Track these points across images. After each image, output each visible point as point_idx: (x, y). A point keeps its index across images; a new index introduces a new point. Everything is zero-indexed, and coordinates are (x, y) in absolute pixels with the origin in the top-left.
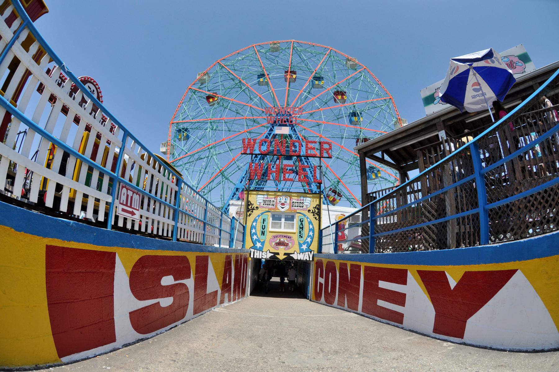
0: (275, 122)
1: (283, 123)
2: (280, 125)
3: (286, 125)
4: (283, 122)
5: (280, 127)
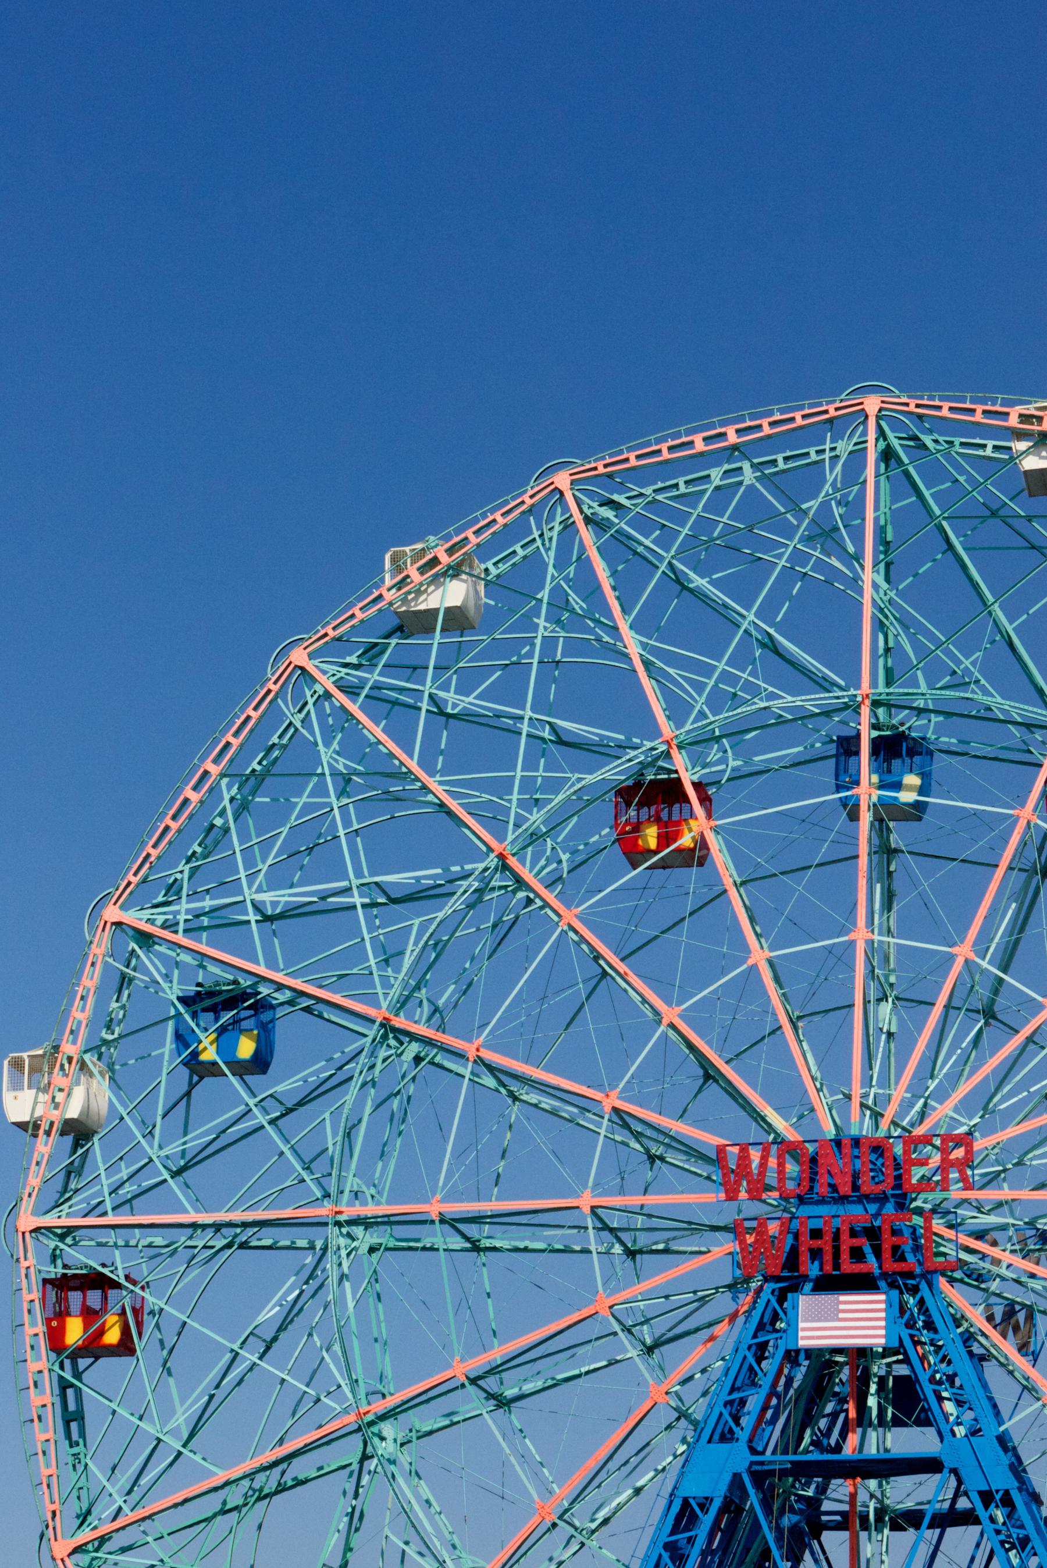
0: (792, 1260)
1: (848, 1266)
2: (827, 1284)
3: (864, 1283)
4: (845, 1256)
5: (825, 1299)
